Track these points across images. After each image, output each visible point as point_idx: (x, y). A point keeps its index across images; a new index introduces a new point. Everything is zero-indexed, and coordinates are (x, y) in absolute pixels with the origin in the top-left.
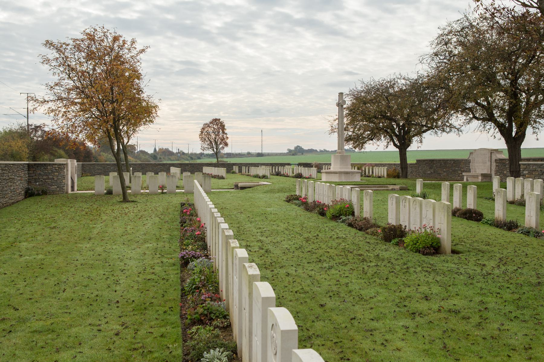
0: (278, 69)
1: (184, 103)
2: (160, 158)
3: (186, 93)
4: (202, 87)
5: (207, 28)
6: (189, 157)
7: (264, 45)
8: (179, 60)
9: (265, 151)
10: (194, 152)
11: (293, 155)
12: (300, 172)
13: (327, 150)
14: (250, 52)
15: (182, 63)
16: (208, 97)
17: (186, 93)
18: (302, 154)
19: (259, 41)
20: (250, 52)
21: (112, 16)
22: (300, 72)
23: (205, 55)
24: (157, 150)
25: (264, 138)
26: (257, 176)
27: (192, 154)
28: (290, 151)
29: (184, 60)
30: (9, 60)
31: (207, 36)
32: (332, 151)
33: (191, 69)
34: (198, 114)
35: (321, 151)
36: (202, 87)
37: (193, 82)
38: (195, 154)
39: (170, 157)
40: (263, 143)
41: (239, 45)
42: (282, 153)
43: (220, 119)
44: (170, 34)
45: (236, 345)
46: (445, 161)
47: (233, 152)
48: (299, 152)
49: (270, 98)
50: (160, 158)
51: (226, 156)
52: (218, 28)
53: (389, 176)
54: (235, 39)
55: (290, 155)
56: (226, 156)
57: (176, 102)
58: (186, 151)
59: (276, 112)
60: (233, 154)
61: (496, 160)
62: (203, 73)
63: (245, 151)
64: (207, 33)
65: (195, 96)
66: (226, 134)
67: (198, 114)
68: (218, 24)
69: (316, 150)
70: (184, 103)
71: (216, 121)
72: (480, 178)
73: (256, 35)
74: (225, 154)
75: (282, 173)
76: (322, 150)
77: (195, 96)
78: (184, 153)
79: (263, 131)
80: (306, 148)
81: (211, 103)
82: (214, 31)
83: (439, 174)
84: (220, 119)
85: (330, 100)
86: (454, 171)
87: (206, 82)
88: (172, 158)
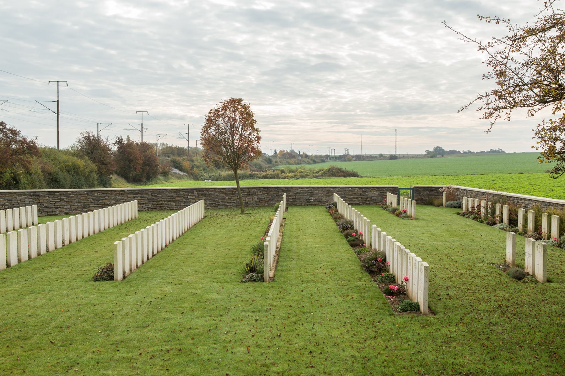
0: (423, 60)
1: (318, 101)
2: (276, 162)
3: (321, 90)
4: (338, 83)
5: (346, 16)
7: (411, 34)
8: (314, 53)
9: (400, 152)
10: (319, 154)
11: (432, 157)
13: (472, 151)
15: (318, 56)
16: (344, 93)
17: (321, 90)
19: (405, 30)
21: (245, 7)
22: (447, 63)
23: (344, 51)
24: (278, 152)
25: (394, 139)
27: (316, 157)
28: (429, 152)
29: (319, 53)
30: (143, 59)
31: (347, 27)
32: (477, 153)
34: (333, 113)
35: (465, 153)
36: (338, 83)
37: (329, 77)
38: (321, 156)
39: (288, 160)
40: (398, 143)
41: (382, 35)
42: (419, 155)
43: (241, 100)
44: (306, 25)
45: (386, 257)
47: (363, 154)
48: (439, 154)
49: (413, 93)
50: (276, 162)
52: (358, 16)
54: (377, 27)
55: (428, 157)
56: (354, 159)
57: (310, 100)
58: (309, 154)
60: (363, 156)
62: (340, 67)
63: (377, 153)
64: (347, 22)
67: (333, 113)
68: (359, 11)
69: (459, 152)
70: (318, 101)
71: (234, 103)
73: (402, 22)
74: (353, 156)
75: (408, 213)
76: (466, 151)
78: (306, 156)
79: (397, 130)
80: (447, 149)
81: (347, 100)
82: (354, 20)
84: (241, 100)
87: (343, 77)
88: (291, 162)
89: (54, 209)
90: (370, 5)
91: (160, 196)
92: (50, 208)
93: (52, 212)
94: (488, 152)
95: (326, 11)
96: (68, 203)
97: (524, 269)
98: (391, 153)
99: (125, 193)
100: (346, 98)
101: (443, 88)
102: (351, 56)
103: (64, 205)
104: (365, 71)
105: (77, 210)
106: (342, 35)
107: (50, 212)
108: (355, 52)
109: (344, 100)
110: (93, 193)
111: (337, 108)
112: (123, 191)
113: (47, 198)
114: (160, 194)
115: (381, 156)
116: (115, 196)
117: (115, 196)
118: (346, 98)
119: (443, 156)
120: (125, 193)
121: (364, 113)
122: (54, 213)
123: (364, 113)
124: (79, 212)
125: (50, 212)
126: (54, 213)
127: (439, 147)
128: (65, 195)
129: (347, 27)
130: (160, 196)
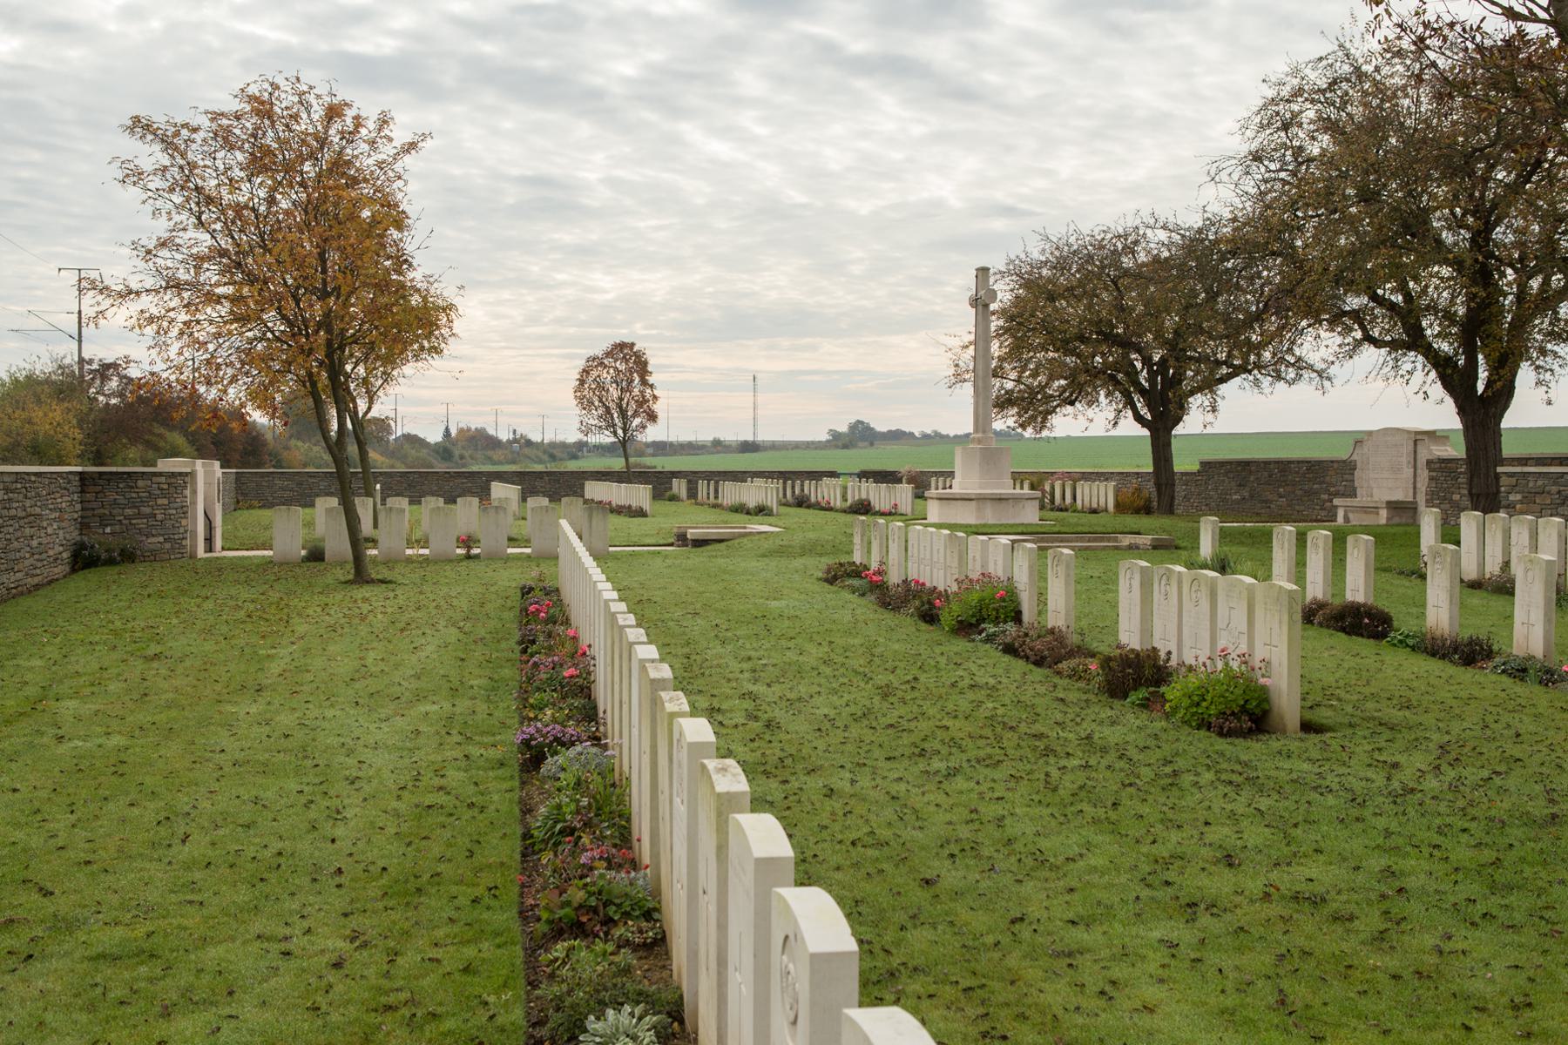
0: (801, 199)
1: (530, 299)
3: (536, 269)
6: (545, 452)
7: (761, 131)
9: (764, 436)
10: (560, 438)
11: (845, 447)
13: (944, 432)
14: (721, 149)
15: (524, 180)
16: (599, 279)
17: (536, 269)
18: (872, 444)
19: (747, 120)
20: (721, 149)
21: (323, 47)
22: (864, 208)
24: (454, 432)
25: (760, 397)
26: (740, 509)
27: (553, 445)
28: (836, 436)
29: (529, 173)
30: (25, 174)
31: (592, 103)
32: (956, 436)
34: (572, 330)
35: (925, 436)
36: (584, 254)
37: (556, 236)
38: (563, 445)
39: (490, 453)
40: (759, 412)
41: (689, 130)
43: (633, 344)
45: (681, 997)
46: (1284, 466)
47: (673, 438)
48: (863, 439)
49: (778, 282)
50: (462, 457)
51: (650, 451)
53: (1120, 507)
55: (837, 447)
56: (650, 451)
57: (506, 295)
59: (796, 323)
60: (671, 444)
61: (1429, 462)
63: (706, 436)
64: (595, 95)
65: (560, 277)
66: (652, 386)
67: (572, 330)
69: (911, 434)
70: (530, 299)
71: (622, 349)
72: (1384, 513)
74: (647, 445)
75: (813, 499)
76: (929, 432)
77: (560, 277)
78: (529, 443)
80: (881, 427)
81: (609, 296)
83: (1266, 502)
84: (633, 344)
85: (949, 289)
86: (1309, 493)
87: (594, 237)
88: (495, 457)
90: (657, 56)
95: (542, 64)
97: (1017, 617)
98: (742, 438)
100: (605, 291)
101: (856, 270)
102: (613, 183)
104: (653, 222)
106: (584, 129)
108: (619, 173)
109: (599, 298)
111: (582, 317)
115: (717, 443)
118: (605, 291)
119: (872, 444)
121: (654, 332)
123: (654, 332)
127: (862, 423)
129: (592, 103)
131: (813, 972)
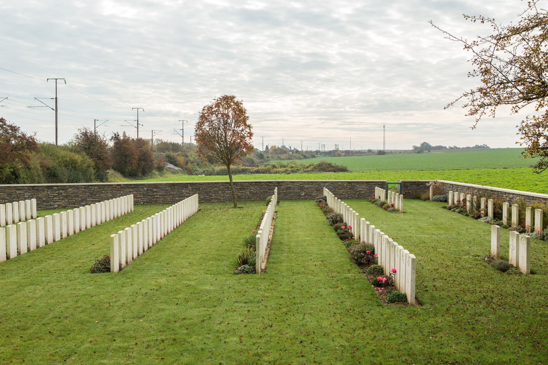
0: (411, 59)
2: (268, 157)
3: (311, 87)
4: (328, 81)
5: (335, 16)
6: (302, 155)
8: (305, 51)
9: (388, 148)
11: (419, 152)
12: (370, 242)
13: (458, 147)
14: (383, 41)
15: (308, 55)
17: (311, 87)
19: (393, 29)
20: (383, 41)
21: (238, 7)
22: (434, 61)
27: (307, 152)
28: (416, 148)
29: (310, 52)
31: (337, 26)
32: (463, 148)
33: (319, 63)
34: (323, 109)
35: (451, 148)
36: (328, 81)
38: (311, 152)
39: (280, 155)
42: (407, 151)
47: (352, 149)
48: (426, 149)
49: (400, 91)
50: (268, 157)
51: (344, 154)
54: (366, 27)
55: (415, 152)
56: (344, 154)
57: (300, 97)
59: (407, 106)
60: (352, 152)
63: (365, 148)
64: (337, 21)
65: (320, 90)
66: (249, 126)
67: (323, 109)
69: (445, 147)
71: (227, 100)
74: (342, 152)
76: (452, 146)
77: (320, 90)
78: (297, 151)
79: (386, 126)
80: (433, 144)
84: (234, 97)
87: (332, 75)
89: (52, 203)
90: (359, 5)
91: (156, 190)
92: (48, 202)
93: (51, 205)
94: (473, 147)
95: (316, 10)
96: (66, 197)
99: (122, 188)
103: (62, 199)
105: (74, 204)
107: (48, 206)
108: (344, 51)
109: (334, 98)
110: (90, 187)
111: (327, 104)
112: (120, 185)
113: (46, 193)
114: (155, 188)
115: (370, 151)
116: (112, 190)
117: (112, 190)
119: (429, 151)
120: (122, 188)
121: (353, 110)
122: (52, 207)
123: (353, 110)
124: (76, 206)
125: (48, 206)
126: (52, 207)
127: (426, 143)
128: (63, 190)
129: (337, 26)
130: (156, 190)
131: (412, 262)
